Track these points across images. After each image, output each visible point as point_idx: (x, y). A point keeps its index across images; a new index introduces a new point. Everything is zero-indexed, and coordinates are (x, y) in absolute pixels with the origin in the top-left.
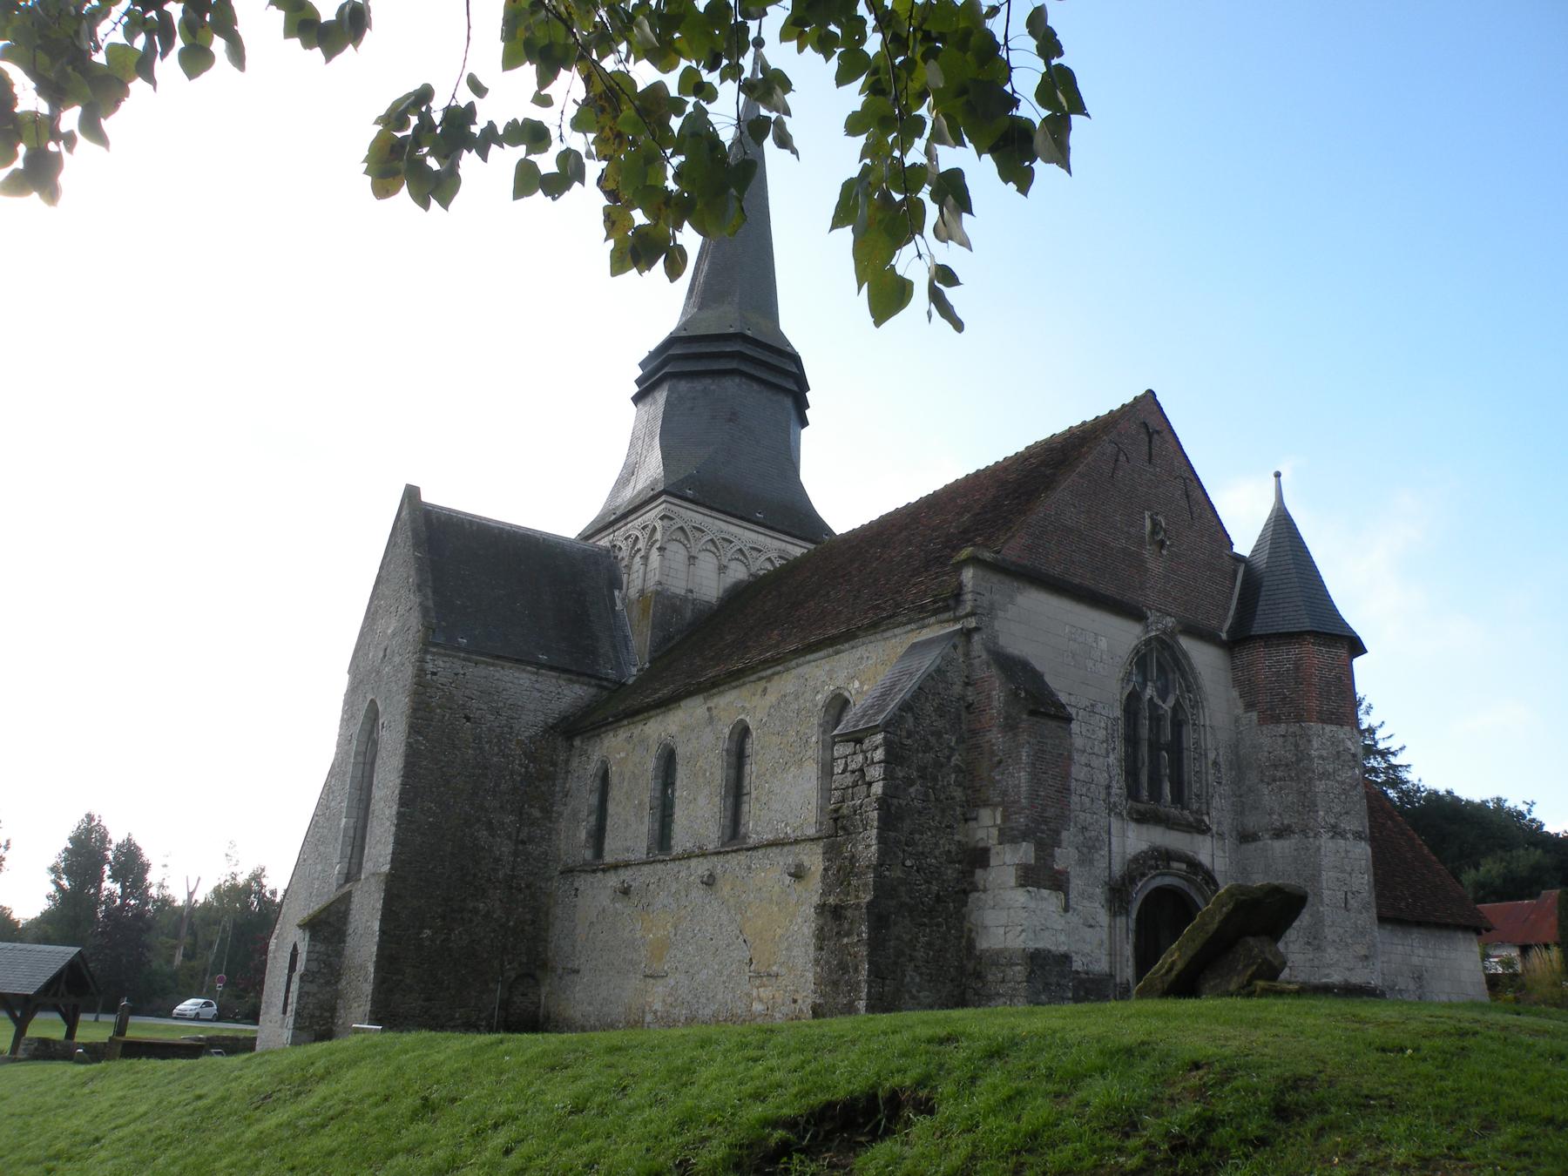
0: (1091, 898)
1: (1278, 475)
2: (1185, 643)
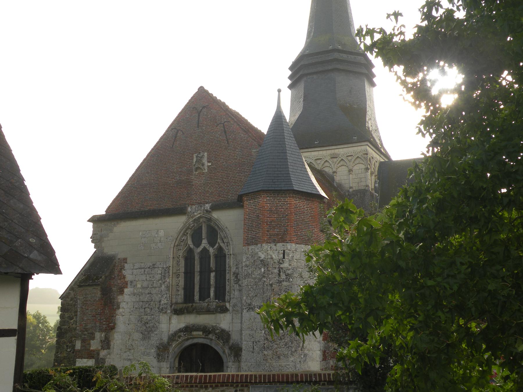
0: (148, 354)
1: (279, 91)
2: (215, 215)
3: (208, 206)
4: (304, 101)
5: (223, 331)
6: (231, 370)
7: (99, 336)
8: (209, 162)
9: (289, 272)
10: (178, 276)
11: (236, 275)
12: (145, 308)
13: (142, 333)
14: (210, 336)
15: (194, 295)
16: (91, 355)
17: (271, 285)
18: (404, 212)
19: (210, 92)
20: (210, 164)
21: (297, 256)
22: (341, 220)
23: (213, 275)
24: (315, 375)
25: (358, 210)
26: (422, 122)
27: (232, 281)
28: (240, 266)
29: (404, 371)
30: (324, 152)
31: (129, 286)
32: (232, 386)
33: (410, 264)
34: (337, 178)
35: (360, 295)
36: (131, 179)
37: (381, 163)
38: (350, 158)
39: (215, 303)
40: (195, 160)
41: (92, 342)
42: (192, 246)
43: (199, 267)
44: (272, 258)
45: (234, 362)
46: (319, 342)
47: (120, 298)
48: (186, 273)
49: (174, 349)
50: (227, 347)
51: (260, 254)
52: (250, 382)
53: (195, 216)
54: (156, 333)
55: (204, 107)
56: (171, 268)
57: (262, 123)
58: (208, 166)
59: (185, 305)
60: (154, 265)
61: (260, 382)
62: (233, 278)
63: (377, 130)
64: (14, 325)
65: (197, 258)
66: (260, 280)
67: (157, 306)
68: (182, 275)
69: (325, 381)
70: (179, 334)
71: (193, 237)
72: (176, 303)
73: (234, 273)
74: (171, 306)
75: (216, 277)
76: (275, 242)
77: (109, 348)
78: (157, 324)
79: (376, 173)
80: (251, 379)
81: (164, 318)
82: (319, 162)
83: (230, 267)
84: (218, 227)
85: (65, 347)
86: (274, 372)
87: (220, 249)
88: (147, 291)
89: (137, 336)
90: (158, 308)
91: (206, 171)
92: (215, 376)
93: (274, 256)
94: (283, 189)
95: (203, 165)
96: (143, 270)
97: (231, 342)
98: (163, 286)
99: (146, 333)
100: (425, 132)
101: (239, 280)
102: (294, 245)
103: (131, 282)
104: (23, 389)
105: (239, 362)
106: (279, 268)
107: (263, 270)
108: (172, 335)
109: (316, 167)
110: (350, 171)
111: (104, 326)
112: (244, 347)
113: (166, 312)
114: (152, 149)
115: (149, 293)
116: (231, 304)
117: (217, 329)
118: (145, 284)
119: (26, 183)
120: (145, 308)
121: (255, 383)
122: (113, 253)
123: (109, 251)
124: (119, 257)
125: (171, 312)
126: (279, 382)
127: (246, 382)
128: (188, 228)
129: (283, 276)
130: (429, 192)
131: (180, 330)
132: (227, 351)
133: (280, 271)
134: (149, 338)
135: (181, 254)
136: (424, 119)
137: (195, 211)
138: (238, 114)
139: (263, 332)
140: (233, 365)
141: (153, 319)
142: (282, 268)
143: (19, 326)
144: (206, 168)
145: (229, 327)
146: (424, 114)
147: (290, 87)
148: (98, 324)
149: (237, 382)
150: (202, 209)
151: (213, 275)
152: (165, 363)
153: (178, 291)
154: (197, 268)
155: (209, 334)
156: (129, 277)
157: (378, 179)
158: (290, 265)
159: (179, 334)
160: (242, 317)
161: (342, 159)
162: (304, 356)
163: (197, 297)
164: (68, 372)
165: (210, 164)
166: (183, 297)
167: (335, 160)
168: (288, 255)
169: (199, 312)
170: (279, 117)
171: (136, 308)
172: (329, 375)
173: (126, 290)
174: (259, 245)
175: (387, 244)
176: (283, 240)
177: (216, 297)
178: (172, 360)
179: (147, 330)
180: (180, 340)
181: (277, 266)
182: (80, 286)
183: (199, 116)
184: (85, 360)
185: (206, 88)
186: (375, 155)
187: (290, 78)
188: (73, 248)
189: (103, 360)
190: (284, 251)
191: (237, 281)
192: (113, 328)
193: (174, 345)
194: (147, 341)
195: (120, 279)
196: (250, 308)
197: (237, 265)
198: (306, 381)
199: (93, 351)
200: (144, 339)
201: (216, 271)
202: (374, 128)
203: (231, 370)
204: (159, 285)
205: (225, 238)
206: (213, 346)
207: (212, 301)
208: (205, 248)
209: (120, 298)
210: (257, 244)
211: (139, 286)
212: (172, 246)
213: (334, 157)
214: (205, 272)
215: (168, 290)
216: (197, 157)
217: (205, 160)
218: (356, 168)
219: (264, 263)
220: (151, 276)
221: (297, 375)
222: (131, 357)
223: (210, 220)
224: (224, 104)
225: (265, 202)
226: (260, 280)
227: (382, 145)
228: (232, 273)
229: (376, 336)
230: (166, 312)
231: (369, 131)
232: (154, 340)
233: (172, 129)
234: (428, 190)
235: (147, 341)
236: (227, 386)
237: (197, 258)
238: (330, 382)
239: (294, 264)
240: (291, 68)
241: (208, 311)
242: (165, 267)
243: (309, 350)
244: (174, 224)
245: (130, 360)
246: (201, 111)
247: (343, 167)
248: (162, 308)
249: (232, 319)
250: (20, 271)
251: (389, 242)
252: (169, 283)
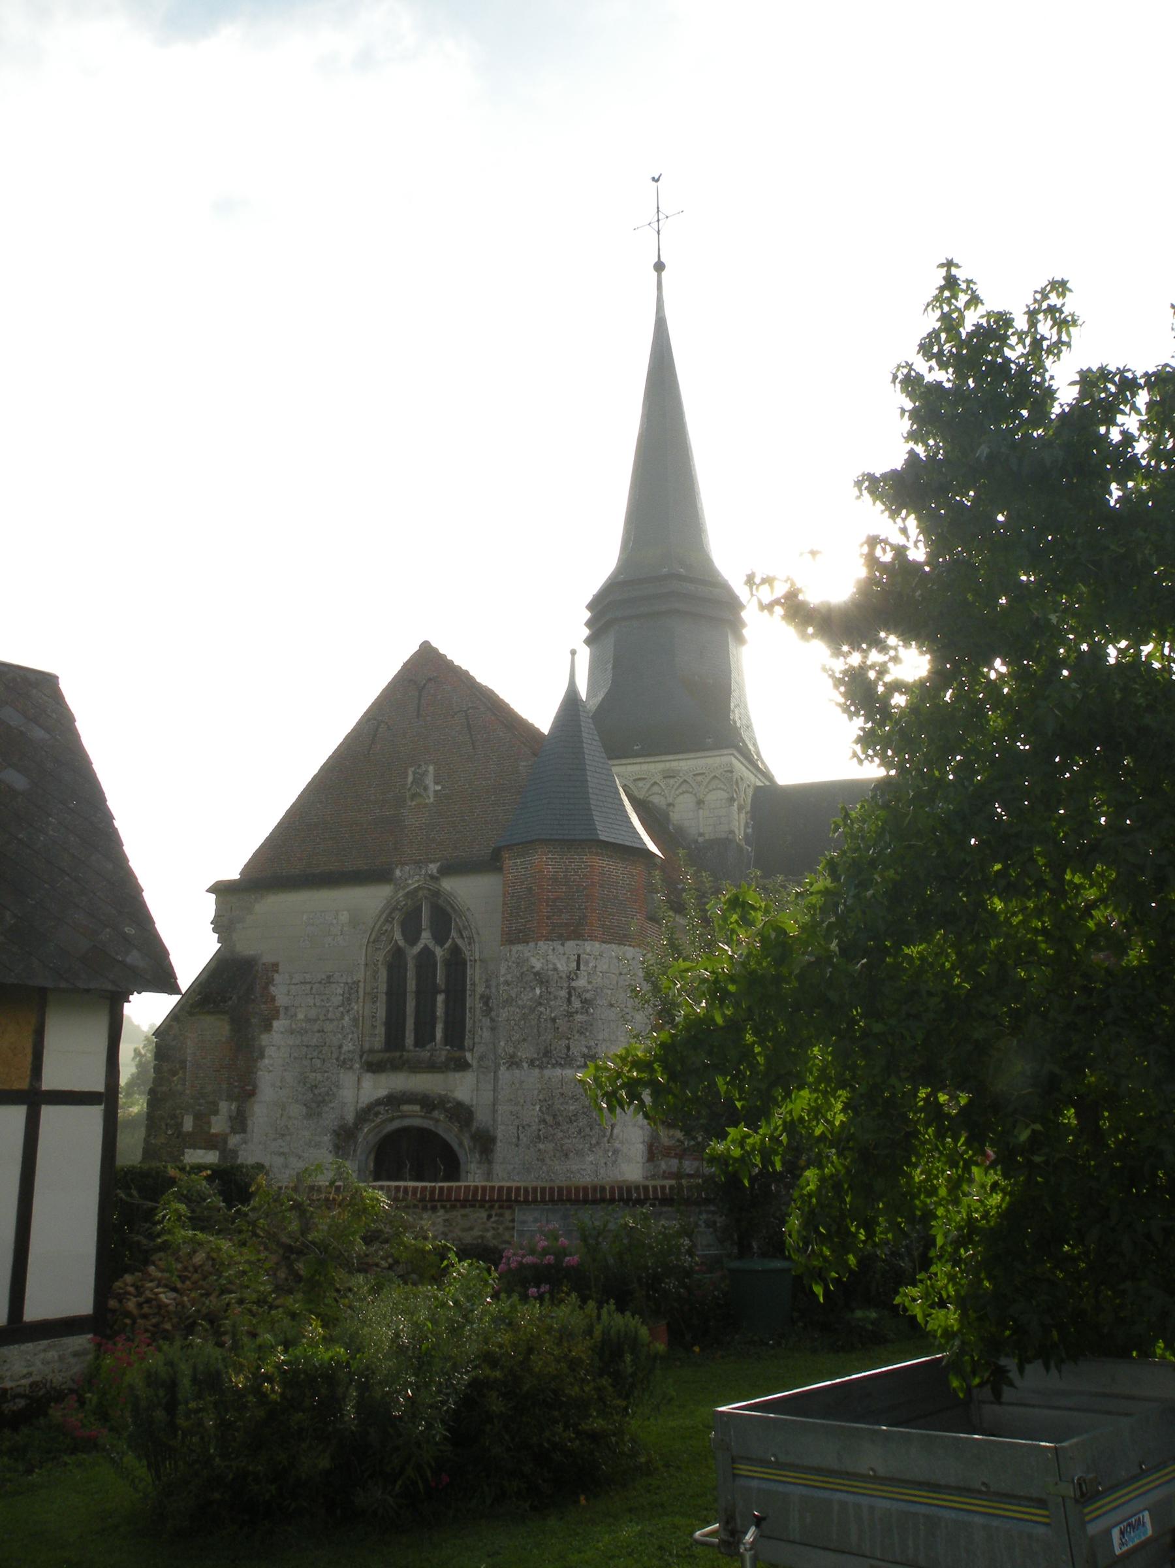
0: (318, 1145)
1: (573, 653)
3: (433, 868)
4: (614, 668)
5: (459, 1104)
6: (474, 1178)
7: (226, 1107)
8: (436, 783)
9: (588, 996)
10: (374, 999)
11: (486, 999)
14: (436, 1114)
15: (404, 1037)
16: (211, 1142)
17: (554, 1020)
18: (836, 905)
19: (442, 651)
20: (438, 788)
21: (603, 966)
22: (733, 920)
23: (440, 998)
24: (637, 1188)
25: (763, 904)
26: (859, 740)
27: (478, 1012)
28: (493, 983)
29: (822, 1179)
30: (652, 766)
31: (282, 1015)
32: (482, 1206)
33: (847, 997)
34: (675, 816)
35: (757, 1049)
36: (289, 812)
37: (757, 788)
38: (699, 778)
39: (444, 1053)
40: (410, 779)
41: (213, 1119)
42: (401, 943)
43: (414, 982)
44: (555, 969)
45: (480, 1162)
46: (642, 1128)
47: (264, 1039)
48: (389, 993)
49: (367, 1135)
51: (534, 961)
52: (517, 1201)
53: (409, 885)
54: (332, 1105)
55: (430, 680)
56: (361, 985)
57: (539, 711)
58: (435, 791)
59: (387, 1055)
60: (329, 977)
61: (535, 1201)
62: (479, 1005)
63: (749, 727)
64: (98, 1085)
65: (411, 965)
66: (532, 1010)
67: (335, 1056)
68: (383, 998)
69: (656, 1198)
70: (376, 1109)
71: (404, 926)
72: (371, 1051)
73: (482, 997)
74: (361, 1057)
75: (447, 1002)
76: (563, 938)
77: (244, 1131)
78: (335, 1090)
79: (748, 808)
80: (518, 1194)
81: (347, 1079)
82: (640, 784)
83: (473, 984)
84: (453, 907)
85: (164, 1127)
86: (558, 1183)
87: (456, 951)
88: (316, 1027)
89: (297, 1110)
90: (337, 1059)
91: (432, 800)
92: (450, 1189)
93: (559, 966)
94: (577, 837)
95: (426, 788)
96: (308, 987)
97: (475, 1125)
98: (347, 1018)
100: (863, 757)
101: (491, 1010)
102: (597, 945)
103: (286, 1008)
104: (129, 1200)
105: (490, 1162)
106: (569, 987)
107: (538, 991)
108: (363, 1110)
109: (636, 793)
110: (700, 803)
111: (236, 1090)
112: (500, 1136)
113: (351, 1068)
114: (330, 758)
115: (319, 1031)
116: (476, 1055)
117: (449, 1102)
118: (313, 1013)
119: (117, 823)
121: (526, 1201)
122: (252, 953)
123: (246, 947)
124: (264, 960)
125: (362, 1067)
126: (569, 1200)
127: (509, 1200)
128: (395, 909)
129: (577, 1004)
130: (876, 868)
131: (379, 1102)
132: (466, 1142)
133: (570, 994)
134: (319, 1114)
135: (381, 959)
136: (862, 733)
137: (411, 878)
138: (492, 692)
139: (538, 1107)
141: (328, 1078)
142: (574, 989)
143: (107, 1086)
144: (431, 795)
145: (472, 1099)
146: (862, 725)
147: (589, 641)
148: (224, 1086)
149: (492, 1200)
150: (423, 872)
151: (440, 998)
153: (374, 1027)
154: (411, 985)
155: (433, 1109)
156: (282, 1000)
157: (753, 818)
158: (590, 983)
159: (376, 1109)
160: (496, 1079)
161: (685, 781)
162: (614, 1153)
163: (410, 1040)
164: (204, 1174)
165: (438, 788)
166: (383, 1039)
167: (672, 781)
168: (587, 963)
169: (415, 1067)
170: (571, 701)
171: (295, 1058)
172: (663, 1187)
173: (275, 1024)
174: (532, 945)
175: (810, 964)
176: (577, 935)
177: (447, 1040)
179: (316, 1100)
181: (566, 985)
182: (191, 1014)
183: (420, 696)
184: (200, 1152)
185: (434, 645)
186: (746, 774)
187: (589, 624)
188: (190, 943)
189: (235, 1153)
190: (579, 956)
191: (488, 1010)
192: (252, 1094)
195: (265, 1003)
196: (514, 1063)
197: (487, 981)
198: (621, 1199)
199: (216, 1135)
200: (309, 1116)
201: (447, 992)
202: (744, 722)
203: (474, 1178)
204: (338, 1015)
205: (465, 928)
206: (441, 1133)
207: (440, 1048)
208: (426, 948)
209: (264, 1039)
210: (527, 943)
211: (301, 1016)
212: (365, 941)
213: (669, 775)
214: (426, 994)
215: (356, 1026)
216: (414, 773)
217: (429, 781)
218: (711, 797)
219: (541, 978)
221: (603, 1189)
222: (286, 1150)
223: (437, 894)
224: (466, 673)
225: (545, 862)
226: (532, 1010)
227: (758, 754)
228: (478, 997)
229: (779, 1116)
230: (351, 1068)
231: (736, 727)
232: (330, 1119)
233: (369, 720)
234: (873, 863)
236: (473, 1206)
237: (411, 965)
238: (667, 1201)
239: (598, 980)
240: (590, 607)
241: (432, 1067)
242: (349, 981)
243: (622, 1143)
244: (370, 900)
245: (283, 1154)
246: (423, 687)
247: (686, 795)
250: (110, 987)
251: (813, 959)
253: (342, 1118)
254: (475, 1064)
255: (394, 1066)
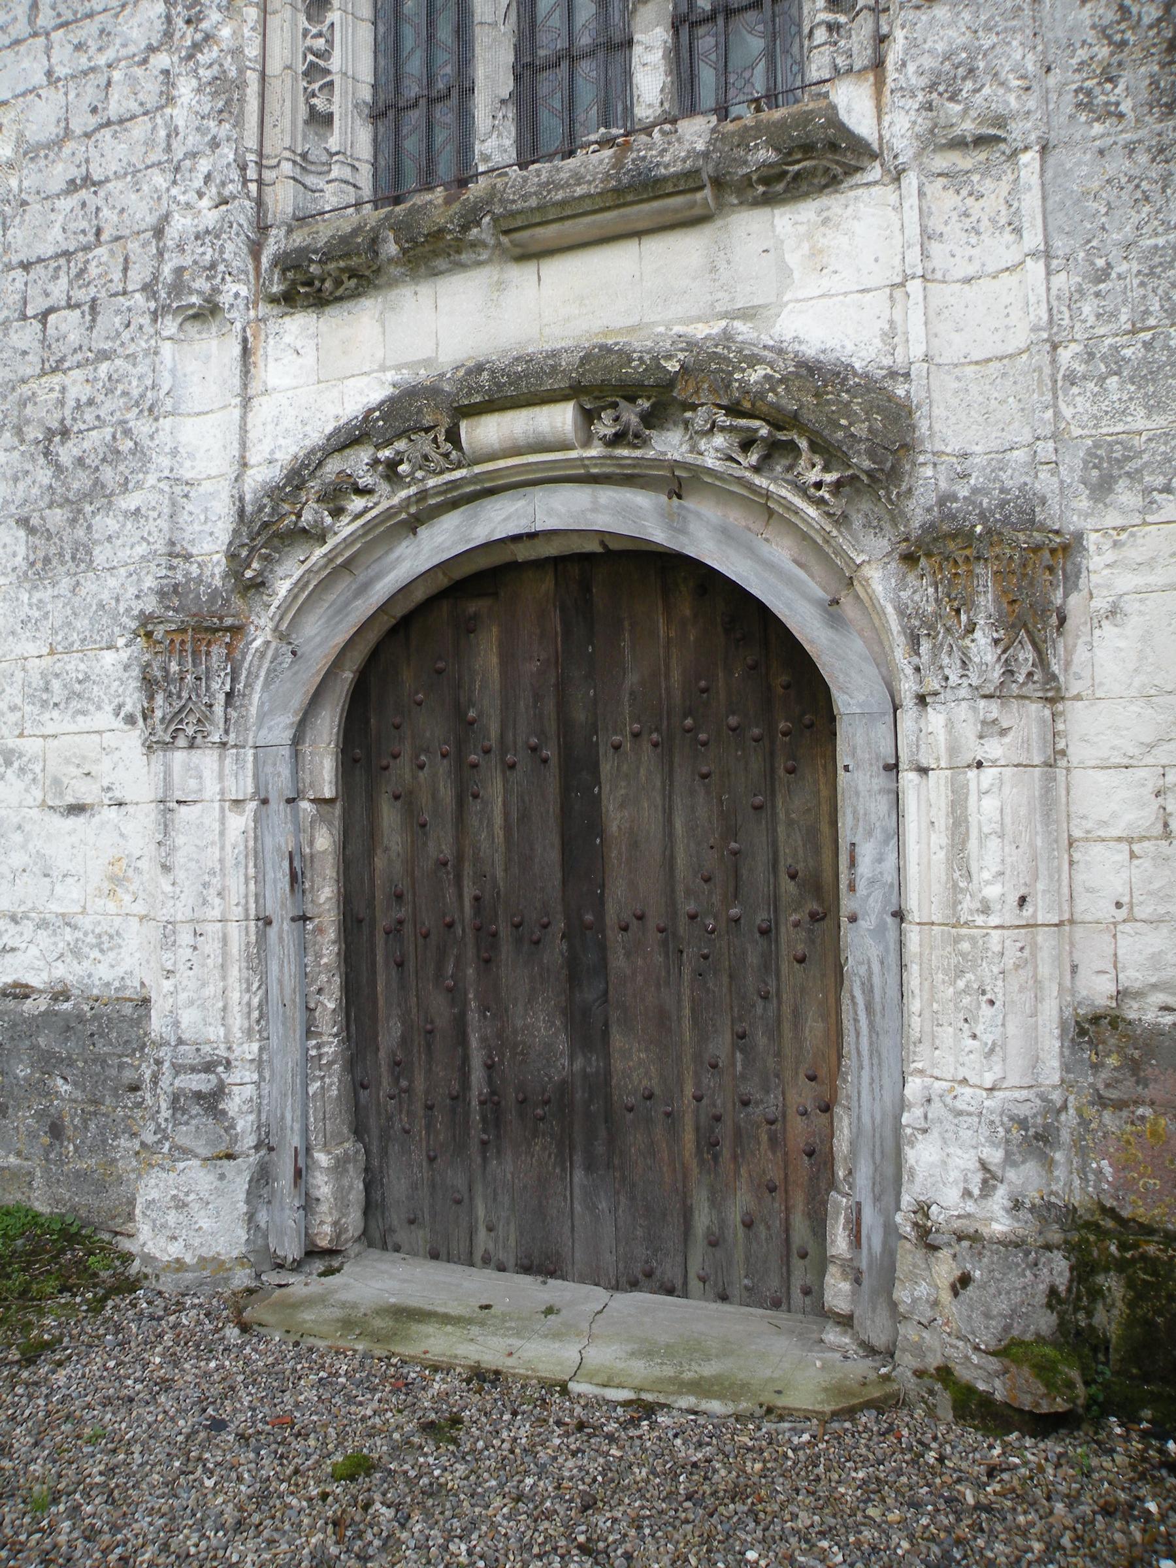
0: (77, 696)
12: (43, 317)
13: (23, 522)
49: (300, 633)
50: (881, 544)
54: (130, 502)
67: (139, 275)
70: (333, 466)
74: (256, 249)
78: (142, 427)
88: (60, 172)
98: (185, 89)
99: (57, 517)
105: (1054, 696)
112: (477, 1357)
115: (72, 186)
120: (43, 317)
131: (349, 438)
134: (82, 554)
140: (990, 728)
145: (891, 334)
152: (207, 760)
153: (320, 120)
169: (528, 235)
178: (280, 730)
180: (345, 528)
193: (283, 588)
194: (65, 583)
204: (151, 89)
220: (89, 30)
232: (124, 572)
235: (65, 583)
248: (179, 271)
249: (927, 235)
252: (237, 52)
253: (176, 553)
254: (900, 128)
255: (432, 252)
